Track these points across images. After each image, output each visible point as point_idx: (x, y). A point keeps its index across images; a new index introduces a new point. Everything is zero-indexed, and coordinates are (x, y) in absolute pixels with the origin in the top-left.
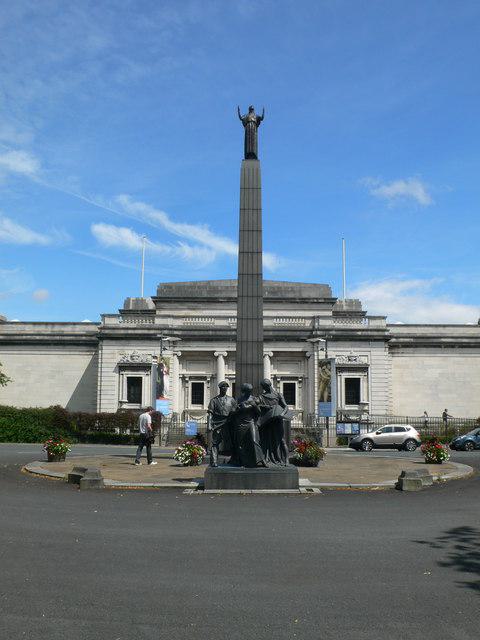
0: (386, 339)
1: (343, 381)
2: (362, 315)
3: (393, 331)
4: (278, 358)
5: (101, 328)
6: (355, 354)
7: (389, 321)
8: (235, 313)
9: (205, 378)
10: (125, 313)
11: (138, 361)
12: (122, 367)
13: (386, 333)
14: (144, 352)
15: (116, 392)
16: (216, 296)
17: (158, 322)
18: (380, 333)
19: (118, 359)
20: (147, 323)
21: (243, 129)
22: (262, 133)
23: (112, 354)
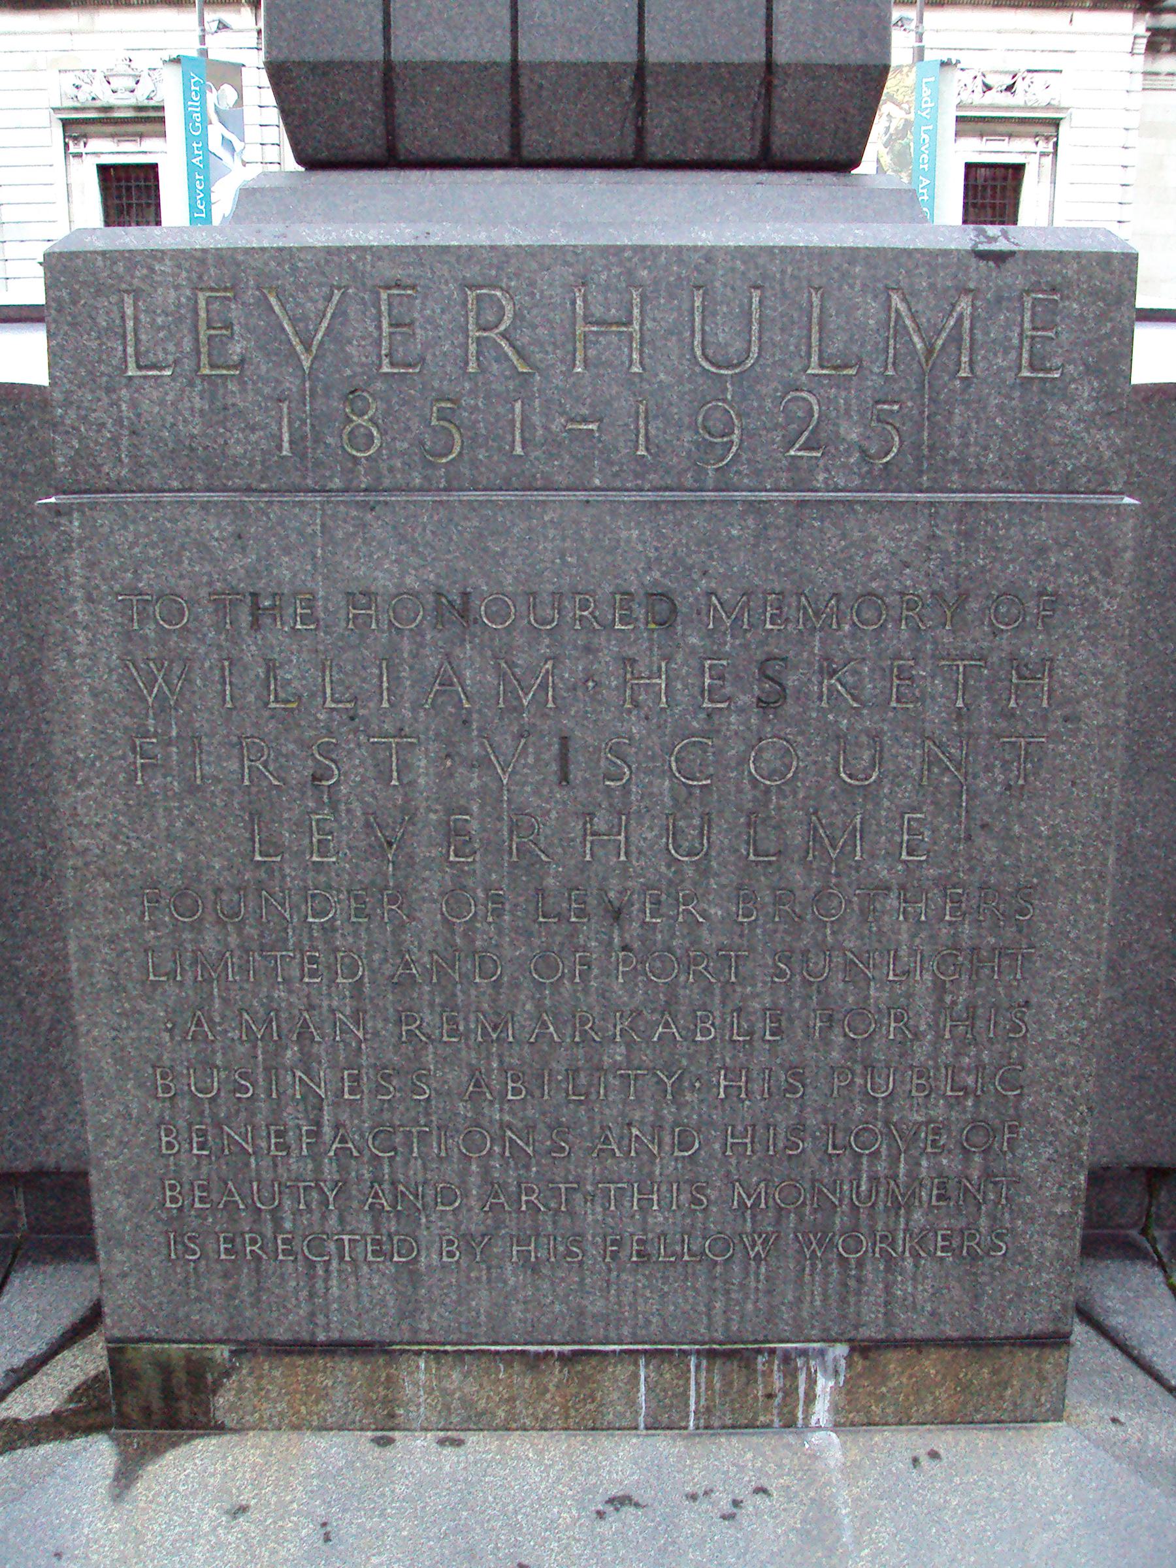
12: (76, 127)
19: (58, 91)
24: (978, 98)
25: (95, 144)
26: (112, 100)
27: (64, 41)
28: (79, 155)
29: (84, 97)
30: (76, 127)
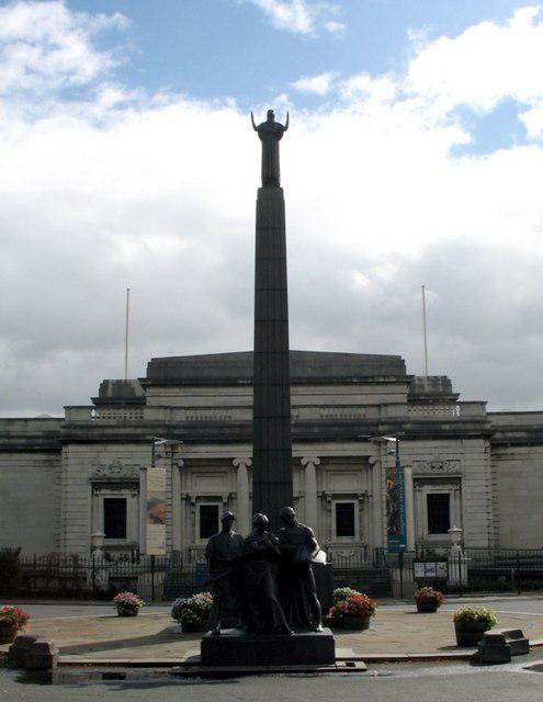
0: (486, 435)
1: (101, 502)
2: (453, 400)
3: (496, 421)
4: (328, 467)
5: (64, 427)
6: (442, 458)
7: (489, 409)
8: (250, 400)
9: (219, 498)
10: (100, 403)
11: (115, 475)
12: (97, 485)
13: (488, 426)
14: (129, 462)
15: (88, 522)
16: (234, 375)
17: (150, 415)
18: (477, 426)
19: (90, 471)
20: (128, 414)
21: (256, 146)
22: (285, 145)
23: (80, 462)
24: (429, 471)
25: (103, 492)
26: (112, 476)
27: (94, 455)
28: (97, 495)
29: (100, 474)
30: (97, 485)
